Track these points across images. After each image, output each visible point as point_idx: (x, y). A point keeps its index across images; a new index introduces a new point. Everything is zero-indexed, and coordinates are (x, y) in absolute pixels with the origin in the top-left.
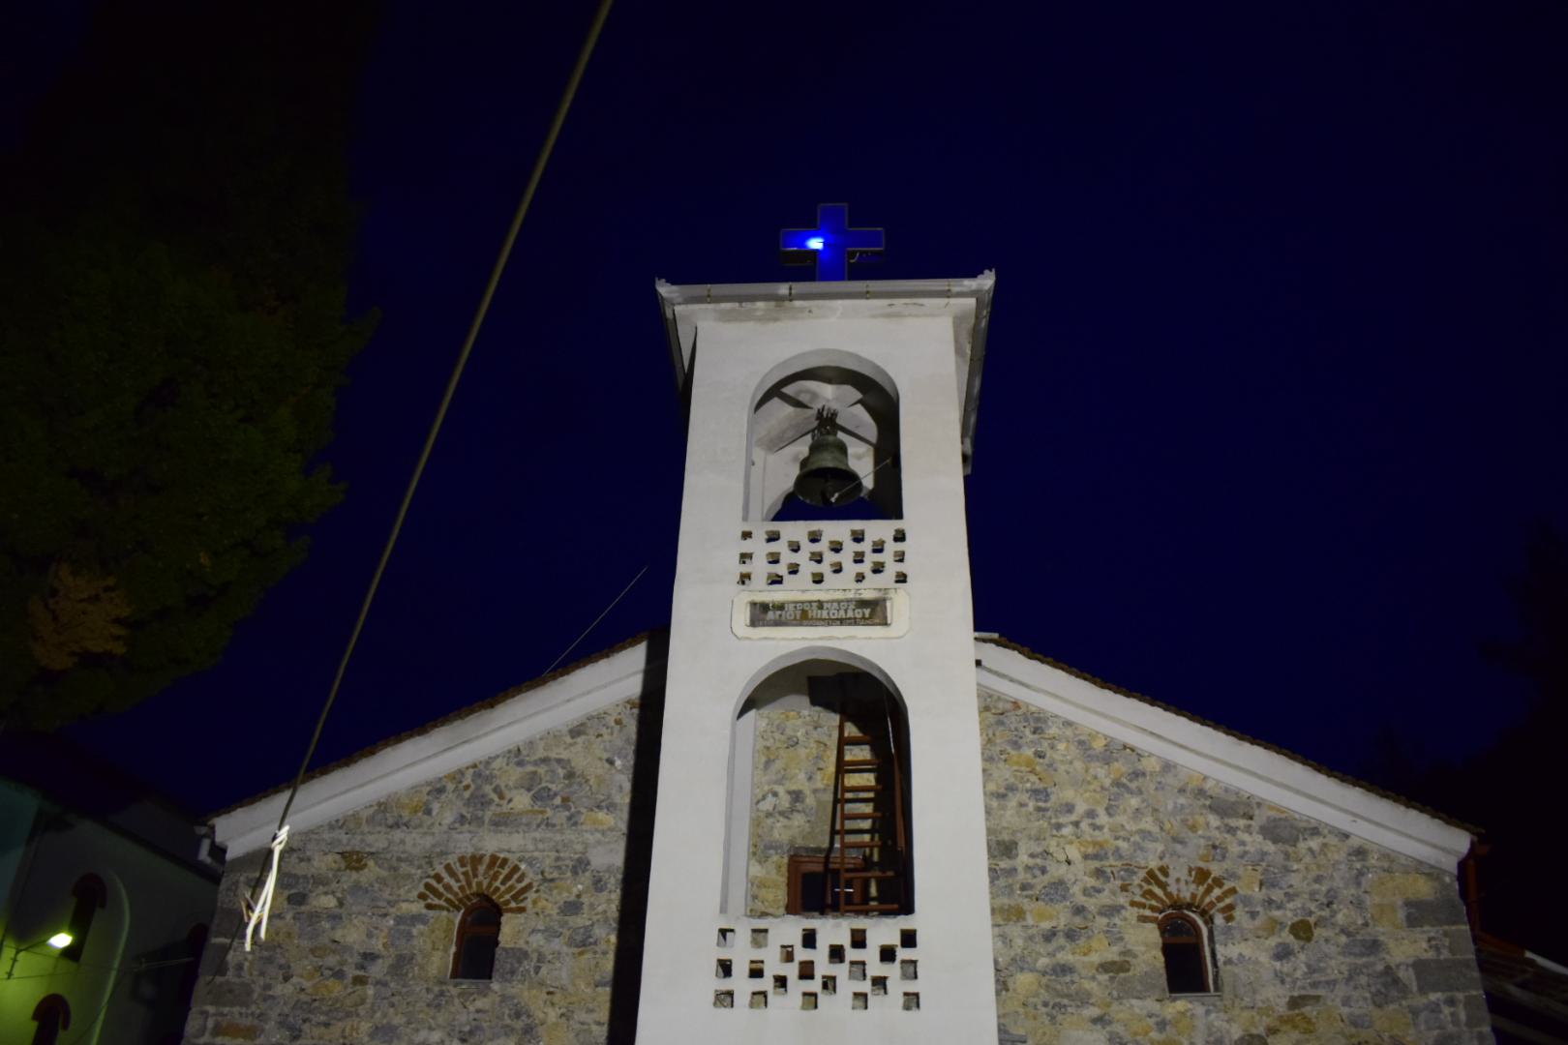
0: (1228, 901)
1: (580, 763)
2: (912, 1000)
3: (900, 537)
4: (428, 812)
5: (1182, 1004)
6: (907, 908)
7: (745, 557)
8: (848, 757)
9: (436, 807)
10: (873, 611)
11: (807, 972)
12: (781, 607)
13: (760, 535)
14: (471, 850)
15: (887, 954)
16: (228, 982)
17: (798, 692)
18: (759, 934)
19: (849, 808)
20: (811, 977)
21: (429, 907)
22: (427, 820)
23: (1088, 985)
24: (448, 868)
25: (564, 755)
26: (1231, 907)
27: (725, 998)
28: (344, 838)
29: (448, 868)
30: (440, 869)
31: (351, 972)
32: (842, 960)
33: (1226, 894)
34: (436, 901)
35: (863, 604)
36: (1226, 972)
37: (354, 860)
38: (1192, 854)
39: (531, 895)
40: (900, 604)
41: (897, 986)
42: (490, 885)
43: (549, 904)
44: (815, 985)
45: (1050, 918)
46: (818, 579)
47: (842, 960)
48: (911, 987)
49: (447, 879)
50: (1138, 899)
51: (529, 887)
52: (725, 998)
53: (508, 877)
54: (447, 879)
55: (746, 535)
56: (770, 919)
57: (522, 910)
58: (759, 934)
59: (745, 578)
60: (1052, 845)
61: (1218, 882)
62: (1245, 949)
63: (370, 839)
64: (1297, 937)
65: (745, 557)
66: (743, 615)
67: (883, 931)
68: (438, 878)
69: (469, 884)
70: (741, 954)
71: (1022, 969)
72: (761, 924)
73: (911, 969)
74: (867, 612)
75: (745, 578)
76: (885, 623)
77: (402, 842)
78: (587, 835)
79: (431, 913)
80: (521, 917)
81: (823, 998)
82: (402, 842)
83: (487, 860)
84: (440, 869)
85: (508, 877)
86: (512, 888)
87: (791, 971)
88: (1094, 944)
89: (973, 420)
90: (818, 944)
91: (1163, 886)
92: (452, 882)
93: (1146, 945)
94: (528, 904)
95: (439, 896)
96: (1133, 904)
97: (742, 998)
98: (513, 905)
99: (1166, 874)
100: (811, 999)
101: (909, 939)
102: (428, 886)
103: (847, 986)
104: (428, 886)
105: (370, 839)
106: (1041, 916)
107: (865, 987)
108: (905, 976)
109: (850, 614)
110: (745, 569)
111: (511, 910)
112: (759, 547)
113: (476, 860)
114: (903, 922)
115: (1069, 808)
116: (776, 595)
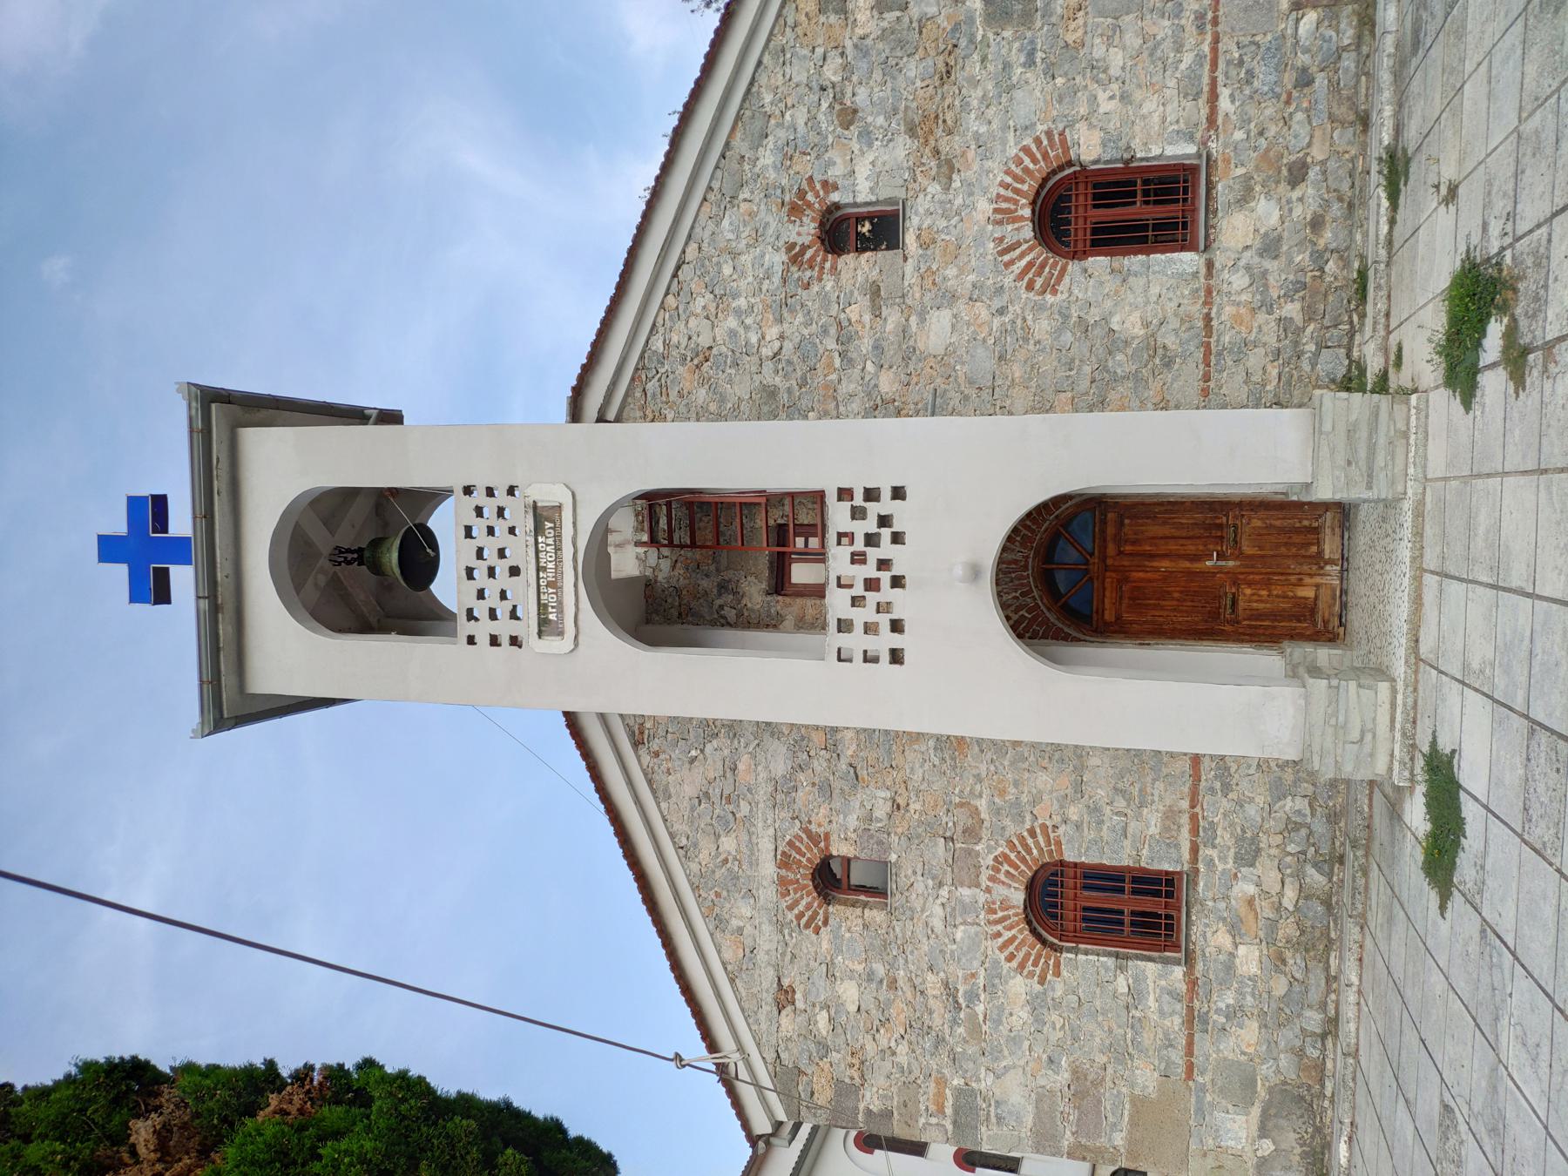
0: (818, 186)
1: (690, 790)
2: (898, 493)
3: (468, 491)
4: (740, 930)
5: (910, 239)
6: (819, 497)
7: (494, 641)
9: (735, 923)
10: (542, 517)
11: (872, 585)
12: (542, 608)
13: (844, 640)
14: (773, 888)
15: (858, 514)
16: (898, 1108)
18: (844, 626)
21: (826, 923)
22: (748, 930)
23: (890, 327)
24: (790, 908)
25: (686, 803)
26: (825, 184)
27: (896, 657)
28: (766, 1008)
29: (790, 908)
30: (790, 916)
31: (884, 994)
32: (864, 554)
33: (813, 188)
34: (821, 917)
35: (538, 530)
36: (884, 194)
37: (784, 997)
38: (773, 220)
39: (813, 828)
40: (549, 493)
41: (886, 505)
42: (805, 867)
43: (820, 819)
44: (885, 577)
46: (514, 571)
48: (886, 494)
49: (801, 907)
50: (815, 273)
51: (807, 832)
52: (896, 657)
53: (799, 851)
54: (801, 907)
55: (471, 640)
56: (829, 616)
57: (827, 835)
58: (844, 626)
59: (514, 641)
60: (767, 352)
61: (801, 194)
62: (863, 170)
63: (765, 985)
64: (851, 123)
66: (552, 645)
68: (800, 916)
69: (805, 886)
70: (483, 629)
72: (833, 625)
73: (871, 495)
74: (548, 525)
75: (514, 641)
77: (767, 953)
78: (760, 779)
79: (831, 921)
80: (834, 837)
81: (896, 571)
82: (767, 953)
83: (783, 872)
84: (790, 916)
85: (799, 851)
86: (808, 847)
87: (873, 598)
91: (804, 248)
92: (804, 903)
93: (858, 267)
94: (821, 831)
95: (816, 914)
96: (820, 279)
97: (896, 641)
98: (822, 845)
99: (794, 245)
100: (897, 582)
101: (845, 494)
102: (807, 926)
103: (886, 549)
104: (807, 926)
105: (765, 985)
106: (830, 365)
107: (886, 533)
108: (877, 499)
109: (550, 541)
110: (505, 641)
111: (827, 847)
113: (782, 882)
114: (831, 498)
115: (733, 334)
116: (529, 612)
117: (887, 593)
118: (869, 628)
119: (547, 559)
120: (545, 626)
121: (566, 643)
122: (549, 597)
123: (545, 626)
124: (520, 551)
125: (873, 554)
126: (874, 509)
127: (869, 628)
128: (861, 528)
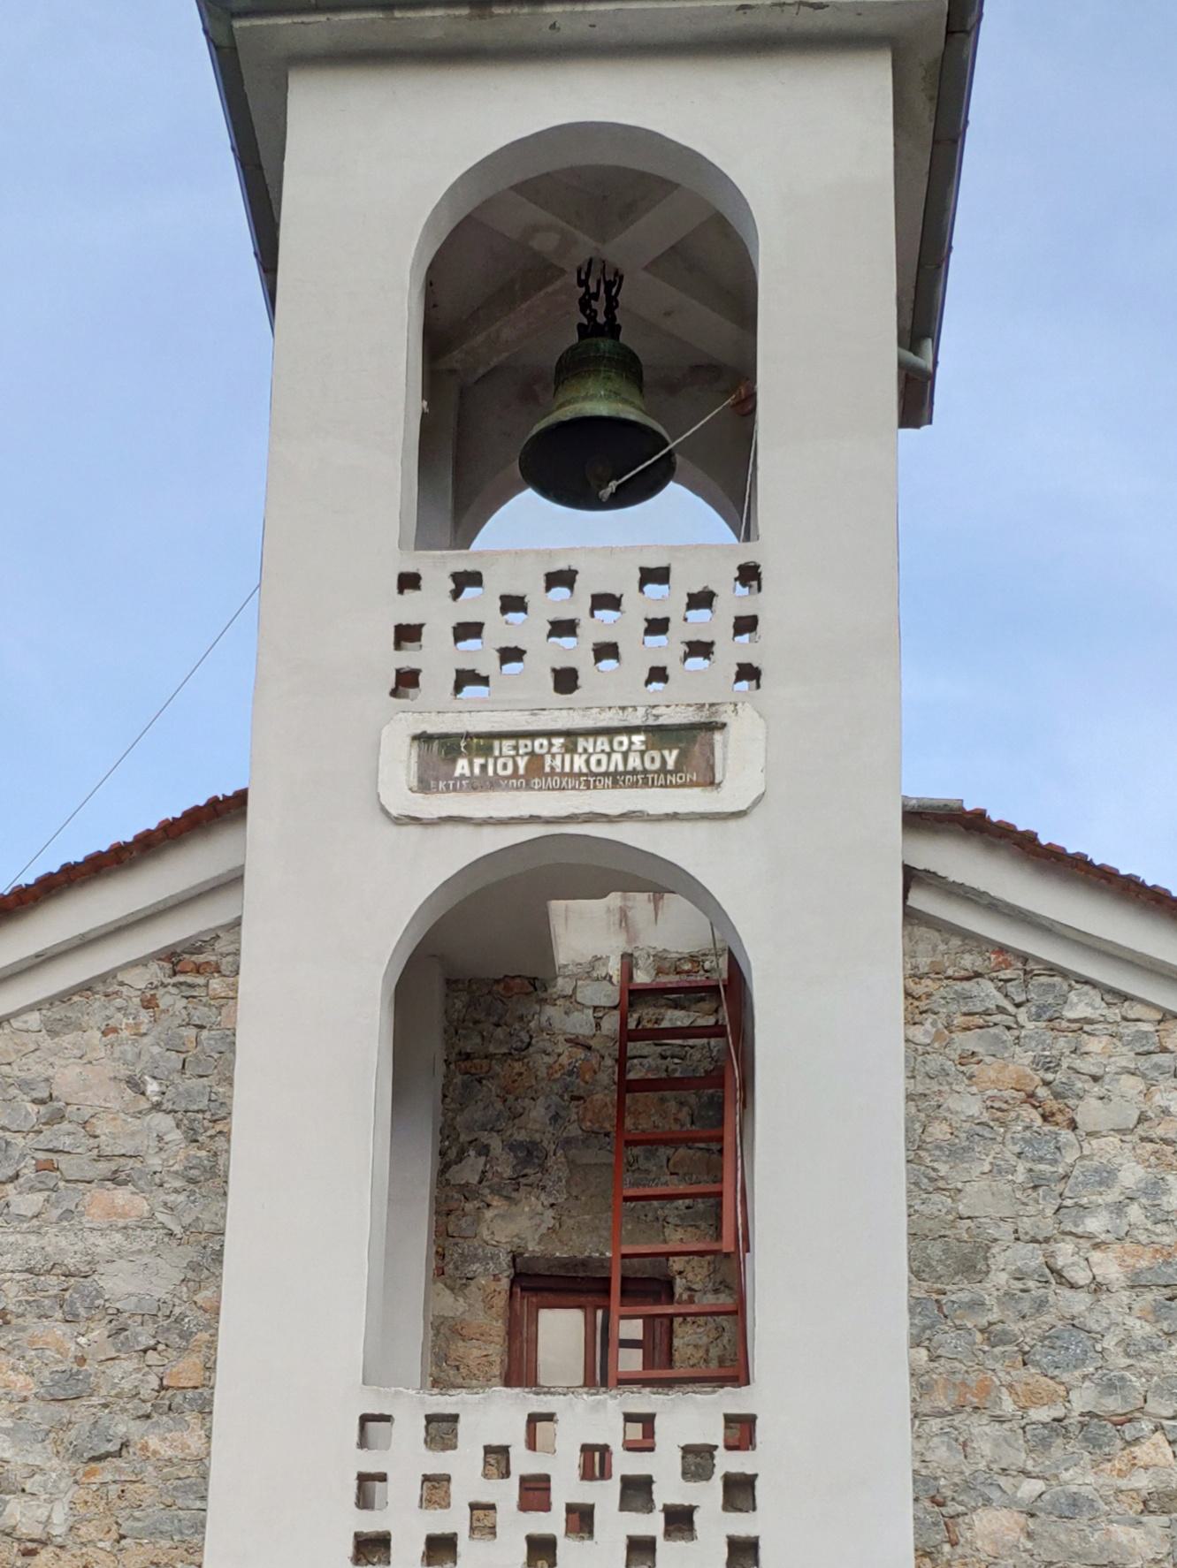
1: (68, 1078)
3: (749, 575)
8: (658, 1321)
10: (688, 744)
12: (483, 743)
17: (521, 490)
18: (441, 1430)
19: (567, 769)
20: (546, 1507)
25: (37, 1070)
32: (605, 1474)
35: (660, 734)
44: (552, 1523)
45: (1051, 1401)
46: (566, 680)
47: (605, 1474)
48: (742, 1525)
55: (409, 582)
58: (441, 1430)
59: (407, 680)
60: (1065, 1253)
65: (407, 634)
66: (398, 767)
67: (690, 1417)
71: (988, 1502)
72: (443, 1403)
73: (740, 1491)
74: (672, 758)
75: (407, 680)
76: (711, 783)
87: (506, 1493)
88: (1142, 1452)
89: (941, 289)
90: (554, 1506)
101: (742, 1430)
109: (634, 762)
112: (434, 608)
114: (732, 1400)
115: (1106, 1176)
116: (473, 714)
117: (516, 1527)
118: (435, 1487)
119: (593, 756)
120: (440, 750)
121: (400, 795)
122: (506, 759)
123: (440, 750)
124: (612, 692)
125: (604, 1496)
126: (707, 1497)
127: (435, 1487)
128: (664, 1468)
